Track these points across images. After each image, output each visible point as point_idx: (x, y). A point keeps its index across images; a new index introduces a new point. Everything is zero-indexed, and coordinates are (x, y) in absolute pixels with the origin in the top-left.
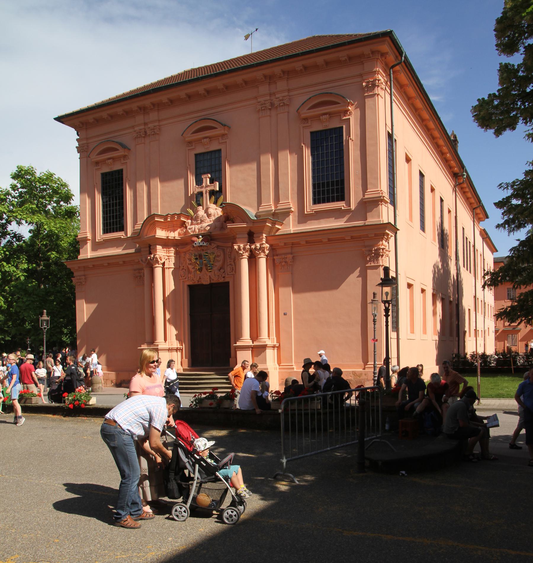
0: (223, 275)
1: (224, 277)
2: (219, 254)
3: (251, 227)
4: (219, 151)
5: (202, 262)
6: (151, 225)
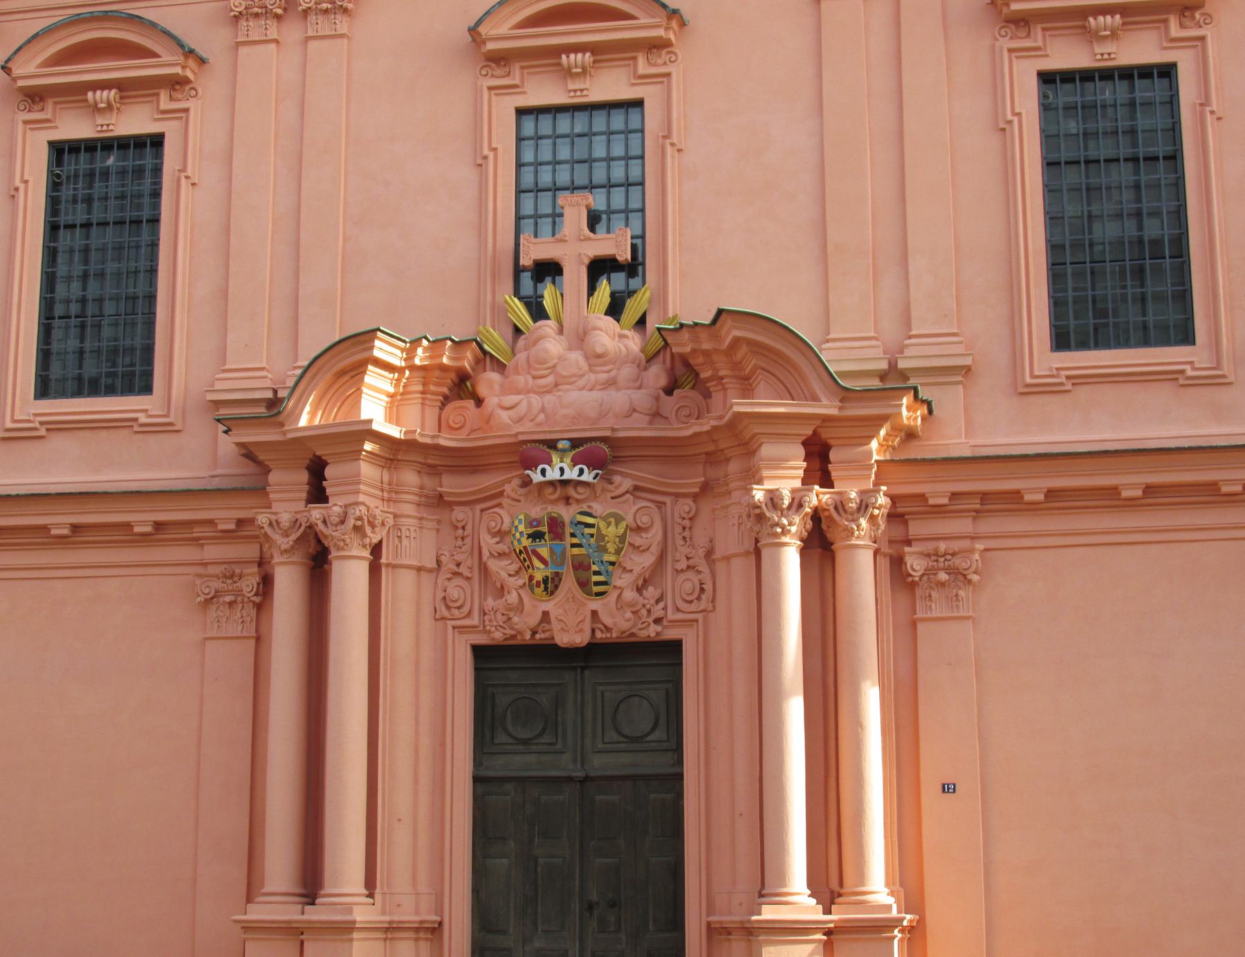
0: (658, 612)
1: (658, 621)
2: (644, 520)
3: (826, 419)
4: (157, 141)
5: (564, 553)
6: (341, 374)
